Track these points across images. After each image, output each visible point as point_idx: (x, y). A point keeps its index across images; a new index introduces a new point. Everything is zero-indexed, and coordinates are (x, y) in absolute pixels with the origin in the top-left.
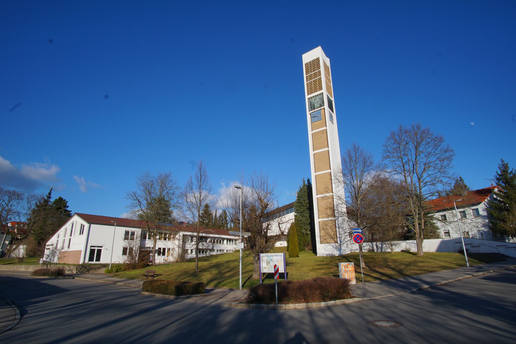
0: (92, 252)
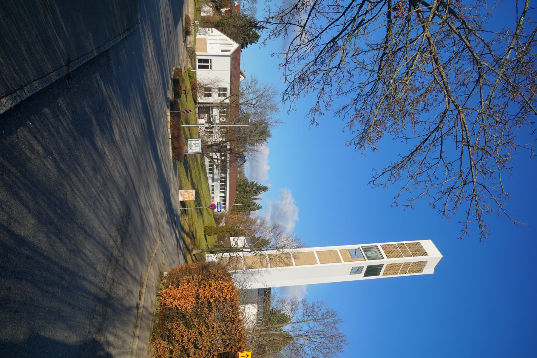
0: (206, 61)
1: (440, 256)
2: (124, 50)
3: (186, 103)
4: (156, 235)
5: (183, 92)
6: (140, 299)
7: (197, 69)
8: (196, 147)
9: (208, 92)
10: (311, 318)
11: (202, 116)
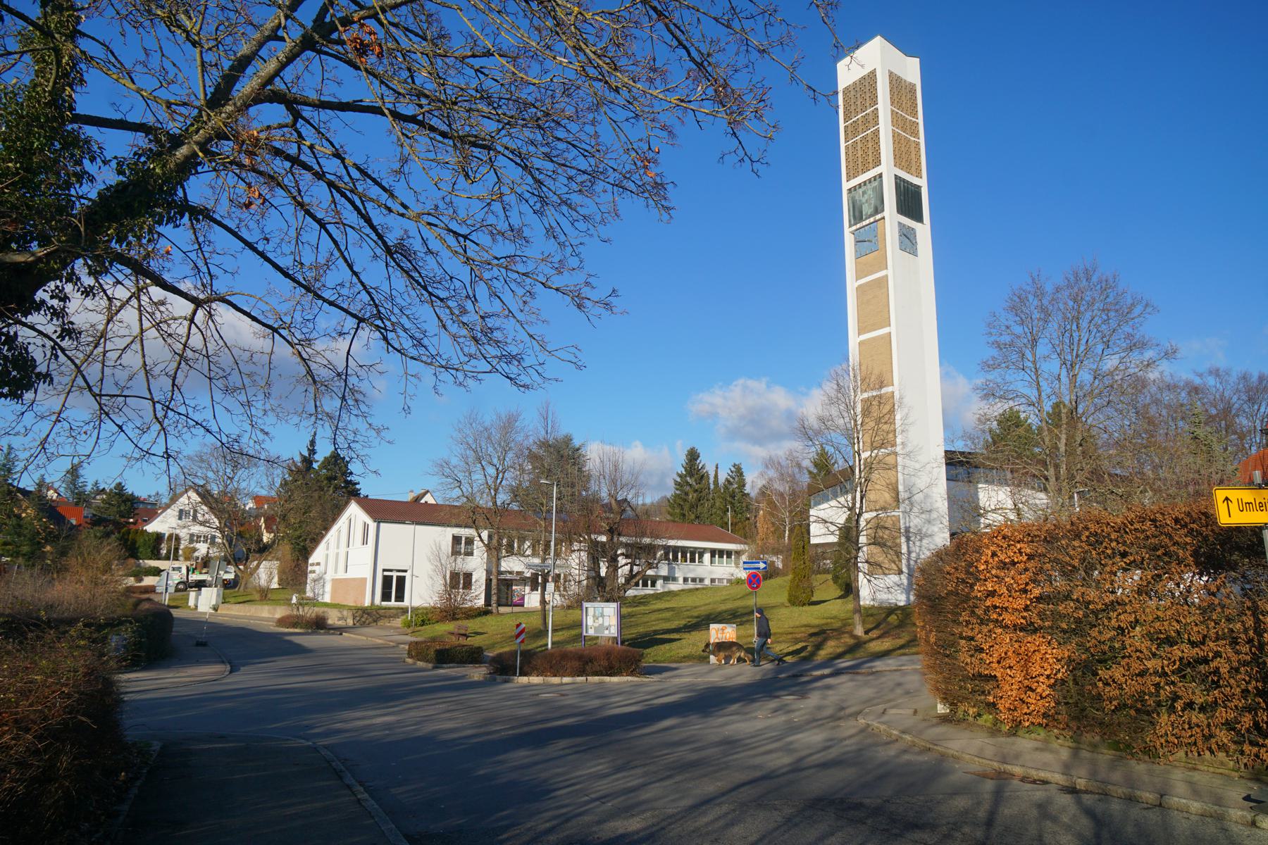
0: (387, 581)
1: (878, 42)
2: (393, 791)
3: (495, 632)
4: (848, 728)
5: (462, 641)
6: (1045, 782)
7: (406, 603)
8: (602, 616)
9: (460, 580)
10: (1029, 355)
11: (516, 599)
